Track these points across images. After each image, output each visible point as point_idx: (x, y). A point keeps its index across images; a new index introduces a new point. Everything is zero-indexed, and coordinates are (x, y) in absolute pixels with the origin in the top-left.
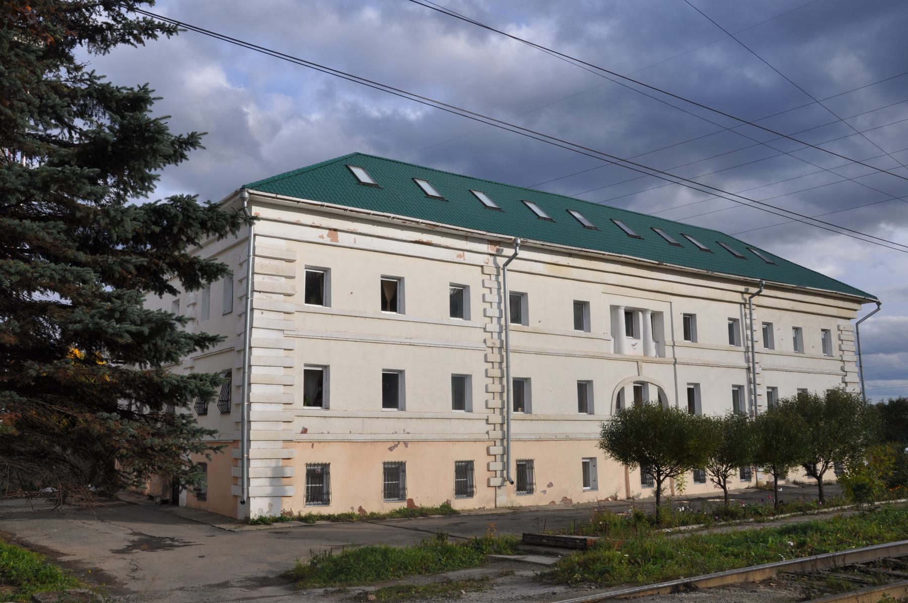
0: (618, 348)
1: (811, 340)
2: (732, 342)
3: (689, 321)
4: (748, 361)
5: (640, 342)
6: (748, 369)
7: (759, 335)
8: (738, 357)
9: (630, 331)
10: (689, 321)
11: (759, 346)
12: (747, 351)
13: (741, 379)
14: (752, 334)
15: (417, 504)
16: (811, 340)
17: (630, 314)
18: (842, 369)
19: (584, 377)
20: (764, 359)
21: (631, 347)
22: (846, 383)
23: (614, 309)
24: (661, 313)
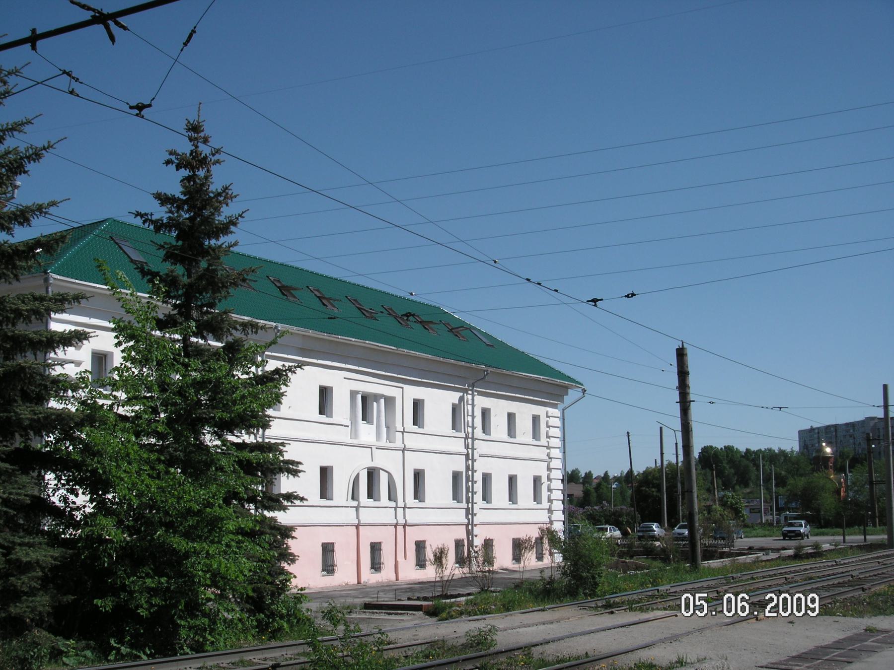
0: (355, 433)
1: (524, 425)
2: (454, 427)
3: (418, 405)
4: (467, 447)
5: (374, 427)
6: (467, 455)
7: (478, 488)
8: (459, 446)
9: (372, 493)
10: (418, 405)
11: (478, 497)
12: (466, 438)
13: (461, 534)
14: (473, 432)
15: (105, 12)
16: (524, 425)
17: (366, 400)
18: (548, 455)
19: (325, 464)
20: (481, 447)
21: (367, 433)
22: (551, 458)
23: (353, 394)
24: (394, 398)
